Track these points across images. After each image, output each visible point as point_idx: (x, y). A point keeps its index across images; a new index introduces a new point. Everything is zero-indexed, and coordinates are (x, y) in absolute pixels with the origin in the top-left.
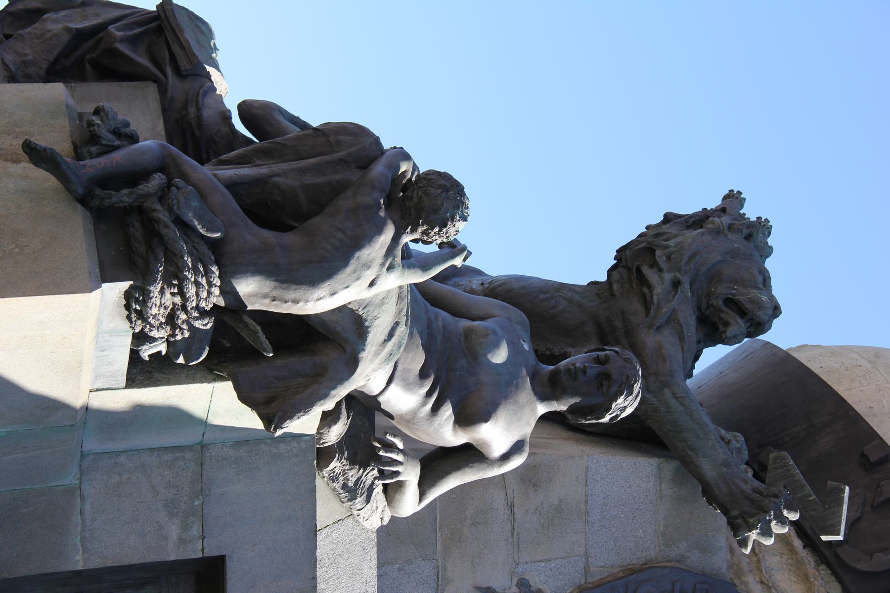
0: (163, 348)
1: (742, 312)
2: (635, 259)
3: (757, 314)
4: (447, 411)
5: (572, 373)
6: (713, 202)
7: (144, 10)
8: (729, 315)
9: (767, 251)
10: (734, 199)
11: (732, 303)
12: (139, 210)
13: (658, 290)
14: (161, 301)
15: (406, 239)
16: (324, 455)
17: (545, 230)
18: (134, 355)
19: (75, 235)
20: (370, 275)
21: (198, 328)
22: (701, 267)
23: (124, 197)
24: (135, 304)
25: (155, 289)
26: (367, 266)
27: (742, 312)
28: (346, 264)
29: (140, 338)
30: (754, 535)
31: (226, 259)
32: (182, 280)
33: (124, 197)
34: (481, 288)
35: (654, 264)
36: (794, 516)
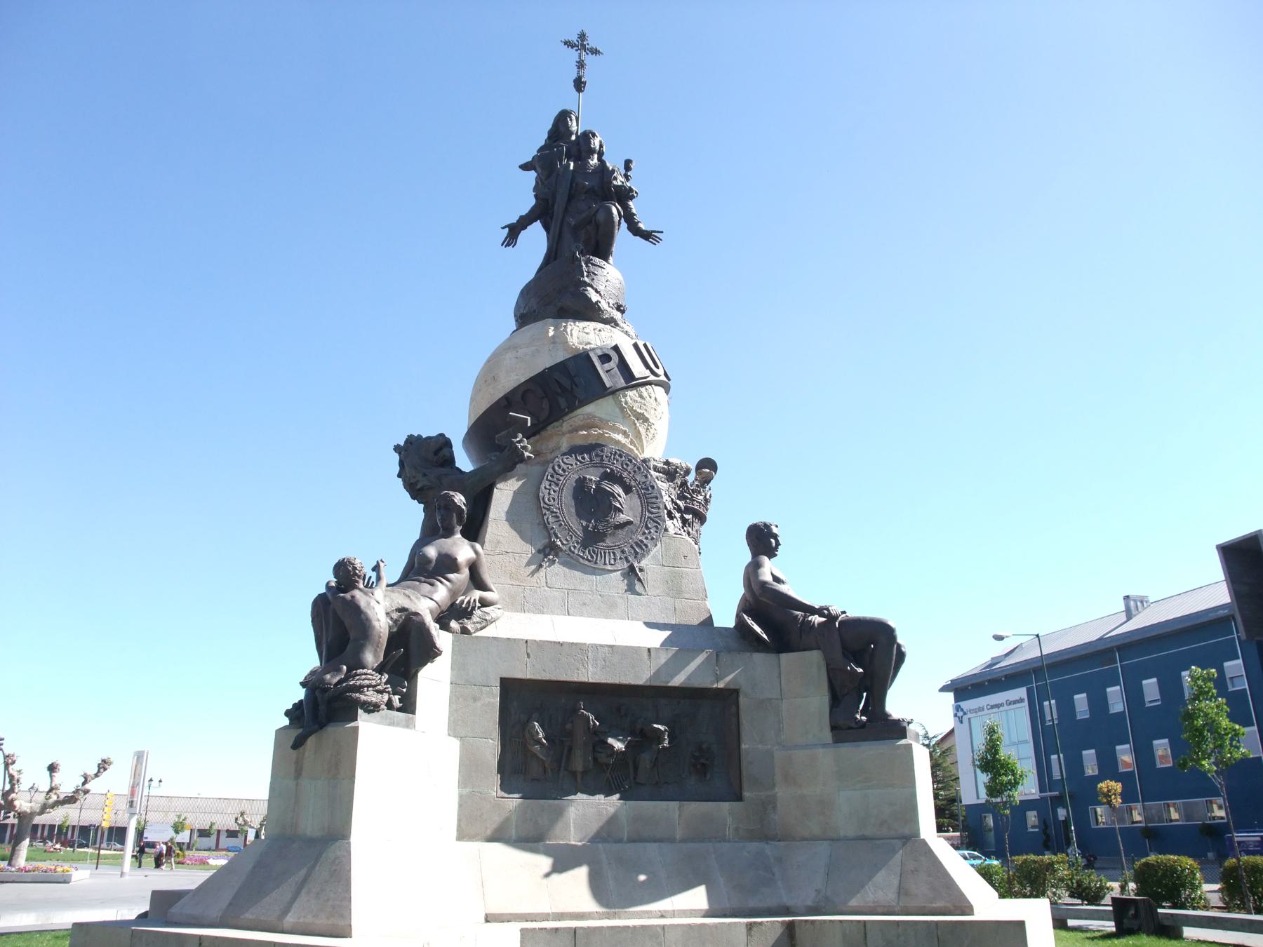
0: (397, 697)
1: (440, 449)
2: (416, 491)
3: (443, 444)
4: (451, 576)
5: (443, 521)
6: (396, 457)
7: (962, 895)
8: (441, 454)
9: (420, 436)
10: (397, 449)
11: (436, 453)
12: (330, 702)
13: (426, 483)
14: (370, 696)
15: (361, 586)
16: (465, 631)
17: (390, 526)
18: (399, 710)
19: (332, 731)
20: (373, 603)
21: (1190, 856)
22: (423, 464)
23: (322, 708)
24: (372, 708)
25: (363, 697)
26: (369, 604)
27: (440, 449)
28: (365, 614)
29: (389, 705)
30: (527, 454)
31: (357, 664)
32: (363, 687)
33: (322, 708)
34: (769, 578)
35: (416, 484)
36: (520, 435)
